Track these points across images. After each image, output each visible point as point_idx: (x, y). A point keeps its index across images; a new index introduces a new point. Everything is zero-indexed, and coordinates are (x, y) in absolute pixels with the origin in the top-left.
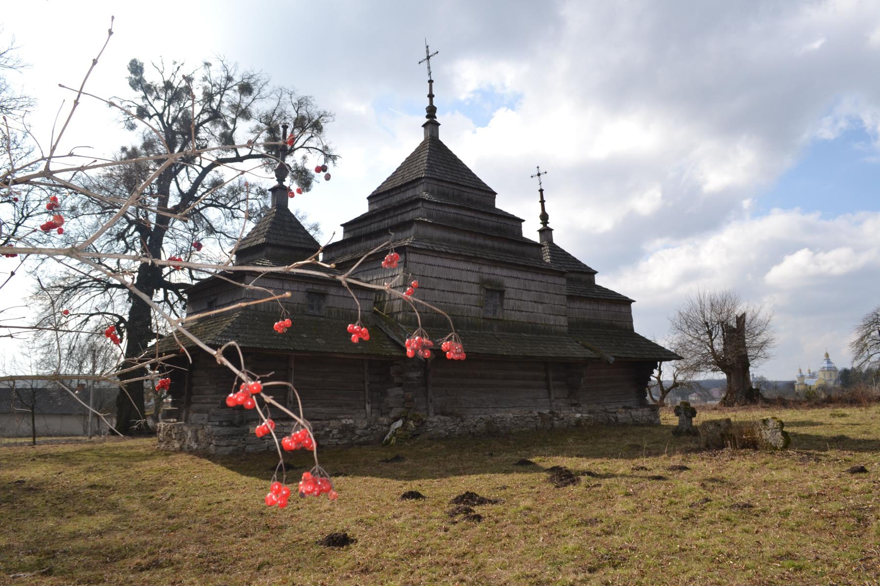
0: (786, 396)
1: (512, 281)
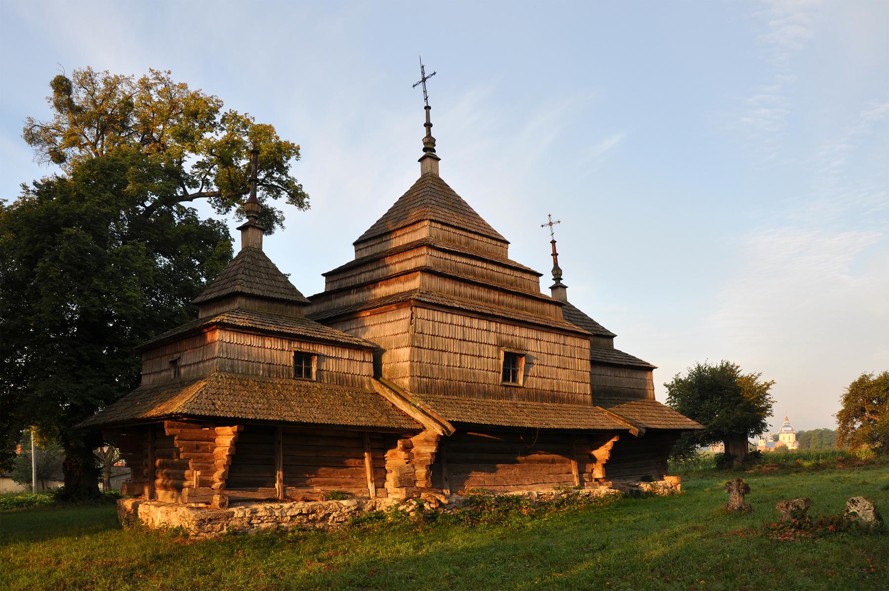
0: (784, 463)
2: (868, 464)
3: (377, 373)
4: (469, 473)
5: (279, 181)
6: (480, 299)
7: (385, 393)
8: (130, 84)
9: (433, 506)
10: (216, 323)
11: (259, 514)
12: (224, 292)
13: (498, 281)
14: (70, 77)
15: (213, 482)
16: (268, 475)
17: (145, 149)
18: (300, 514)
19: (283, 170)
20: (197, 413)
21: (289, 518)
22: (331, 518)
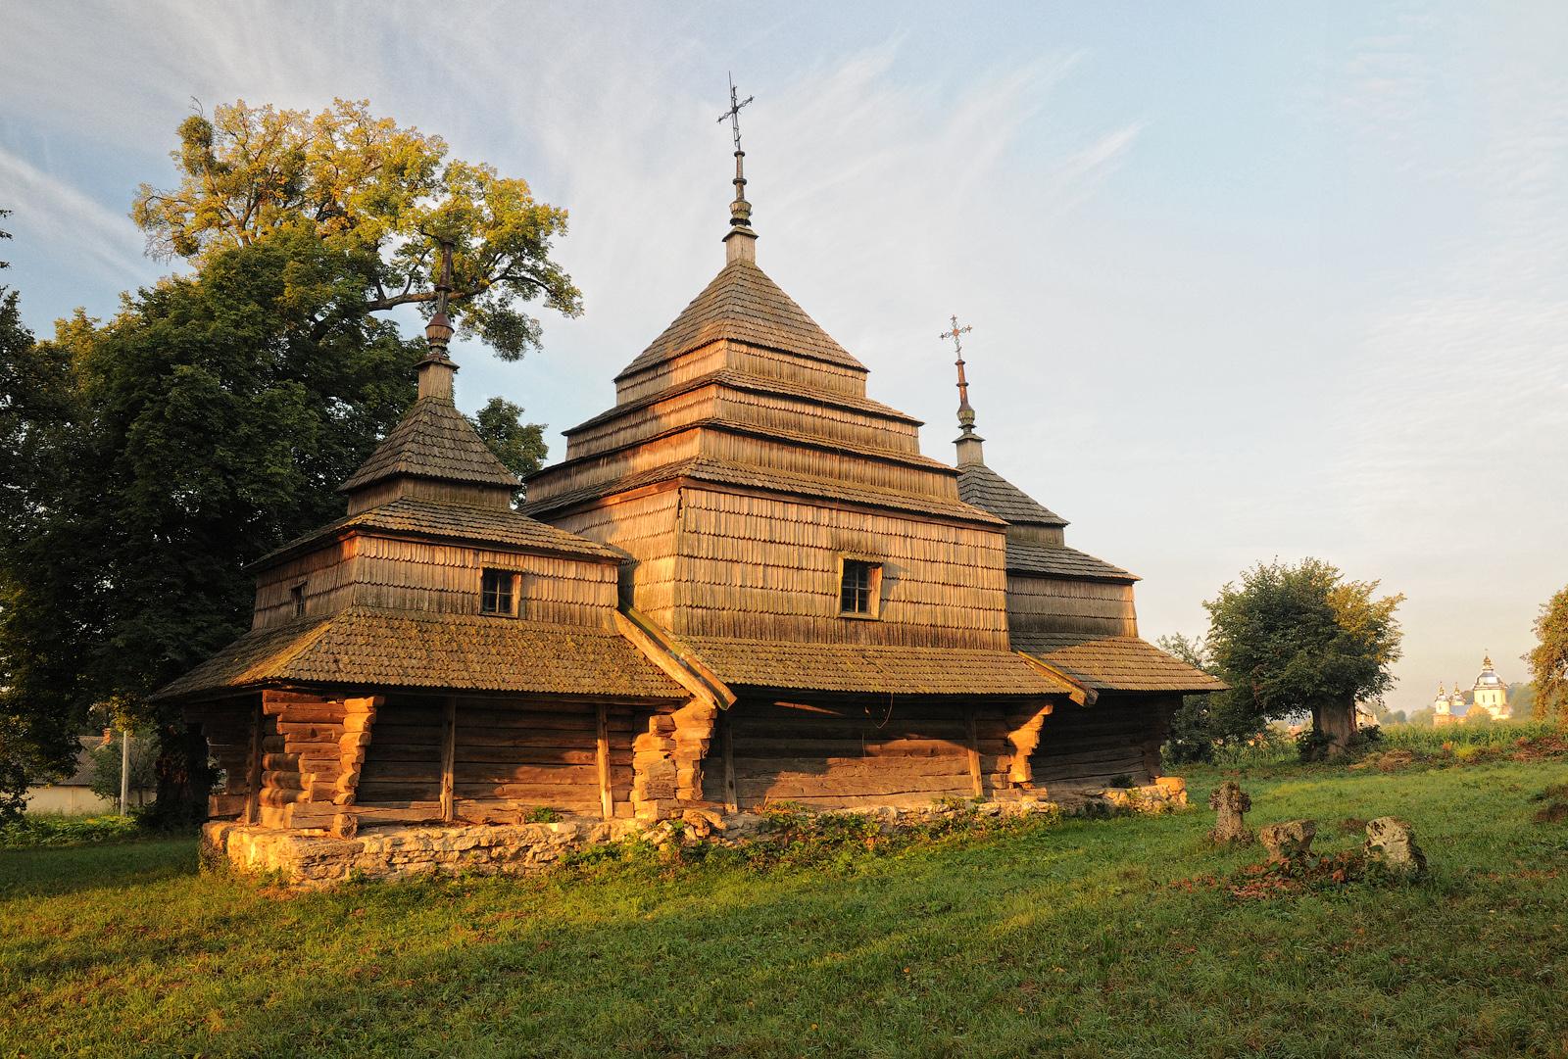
0: (1425, 751)
5: (533, 271)
6: (807, 470)
7: (634, 635)
8: (303, 125)
9: (700, 833)
10: (356, 527)
11: (406, 848)
12: (382, 473)
13: (843, 437)
14: (210, 117)
15: (335, 793)
16: (430, 779)
19: (536, 249)
20: (306, 676)
21: (457, 854)
22: (530, 854)
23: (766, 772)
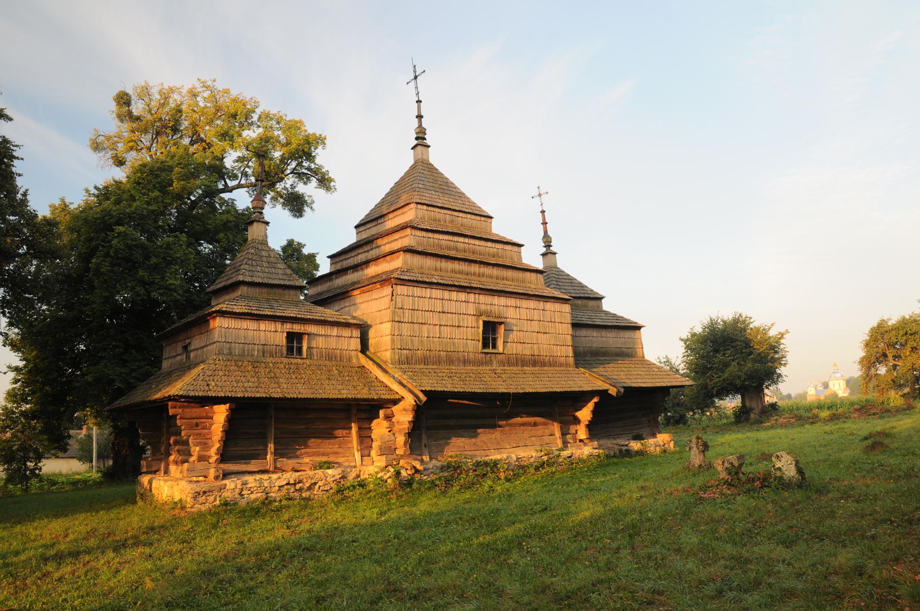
1: (508, 310)
2: (898, 411)
3: (364, 347)
4: (450, 438)
5: (309, 169)
6: (461, 272)
7: (369, 365)
8: (180, 93)
9: (409, 472)
10: (216, 312)
11: (249, 486)
12: (230, 282)
14: (130, 91)
15: (210, 457)
16: (261, 448)
17: (192, 149)
18: (287, 484)
19: (310, 157)
20: (192, 394)
22: (317, 487)
23: (444, 438)
